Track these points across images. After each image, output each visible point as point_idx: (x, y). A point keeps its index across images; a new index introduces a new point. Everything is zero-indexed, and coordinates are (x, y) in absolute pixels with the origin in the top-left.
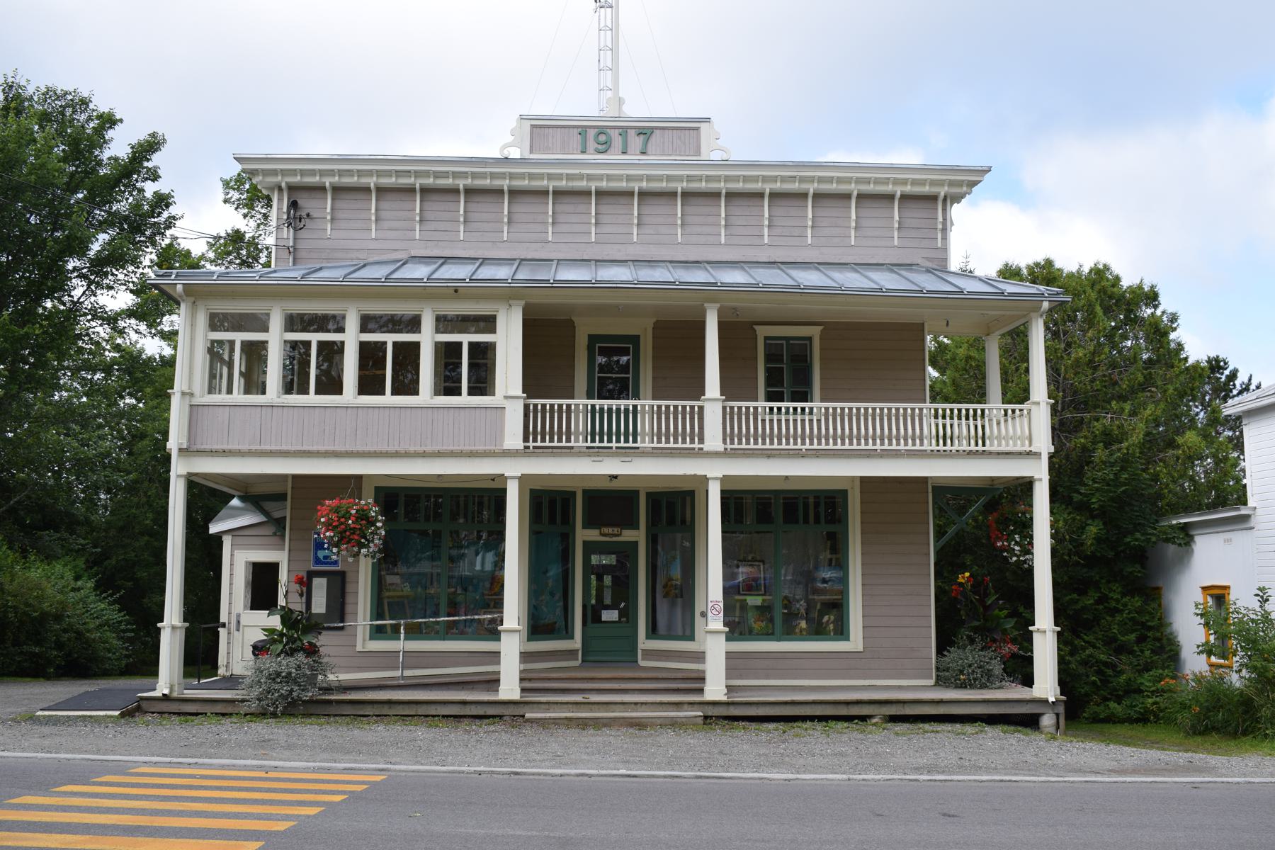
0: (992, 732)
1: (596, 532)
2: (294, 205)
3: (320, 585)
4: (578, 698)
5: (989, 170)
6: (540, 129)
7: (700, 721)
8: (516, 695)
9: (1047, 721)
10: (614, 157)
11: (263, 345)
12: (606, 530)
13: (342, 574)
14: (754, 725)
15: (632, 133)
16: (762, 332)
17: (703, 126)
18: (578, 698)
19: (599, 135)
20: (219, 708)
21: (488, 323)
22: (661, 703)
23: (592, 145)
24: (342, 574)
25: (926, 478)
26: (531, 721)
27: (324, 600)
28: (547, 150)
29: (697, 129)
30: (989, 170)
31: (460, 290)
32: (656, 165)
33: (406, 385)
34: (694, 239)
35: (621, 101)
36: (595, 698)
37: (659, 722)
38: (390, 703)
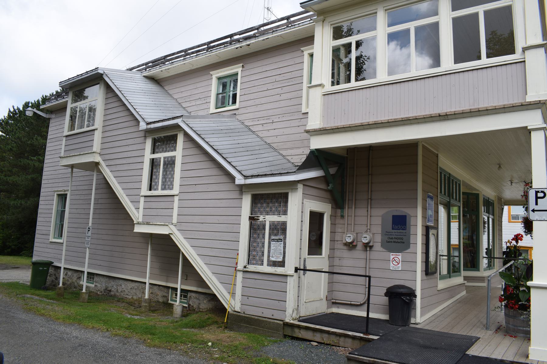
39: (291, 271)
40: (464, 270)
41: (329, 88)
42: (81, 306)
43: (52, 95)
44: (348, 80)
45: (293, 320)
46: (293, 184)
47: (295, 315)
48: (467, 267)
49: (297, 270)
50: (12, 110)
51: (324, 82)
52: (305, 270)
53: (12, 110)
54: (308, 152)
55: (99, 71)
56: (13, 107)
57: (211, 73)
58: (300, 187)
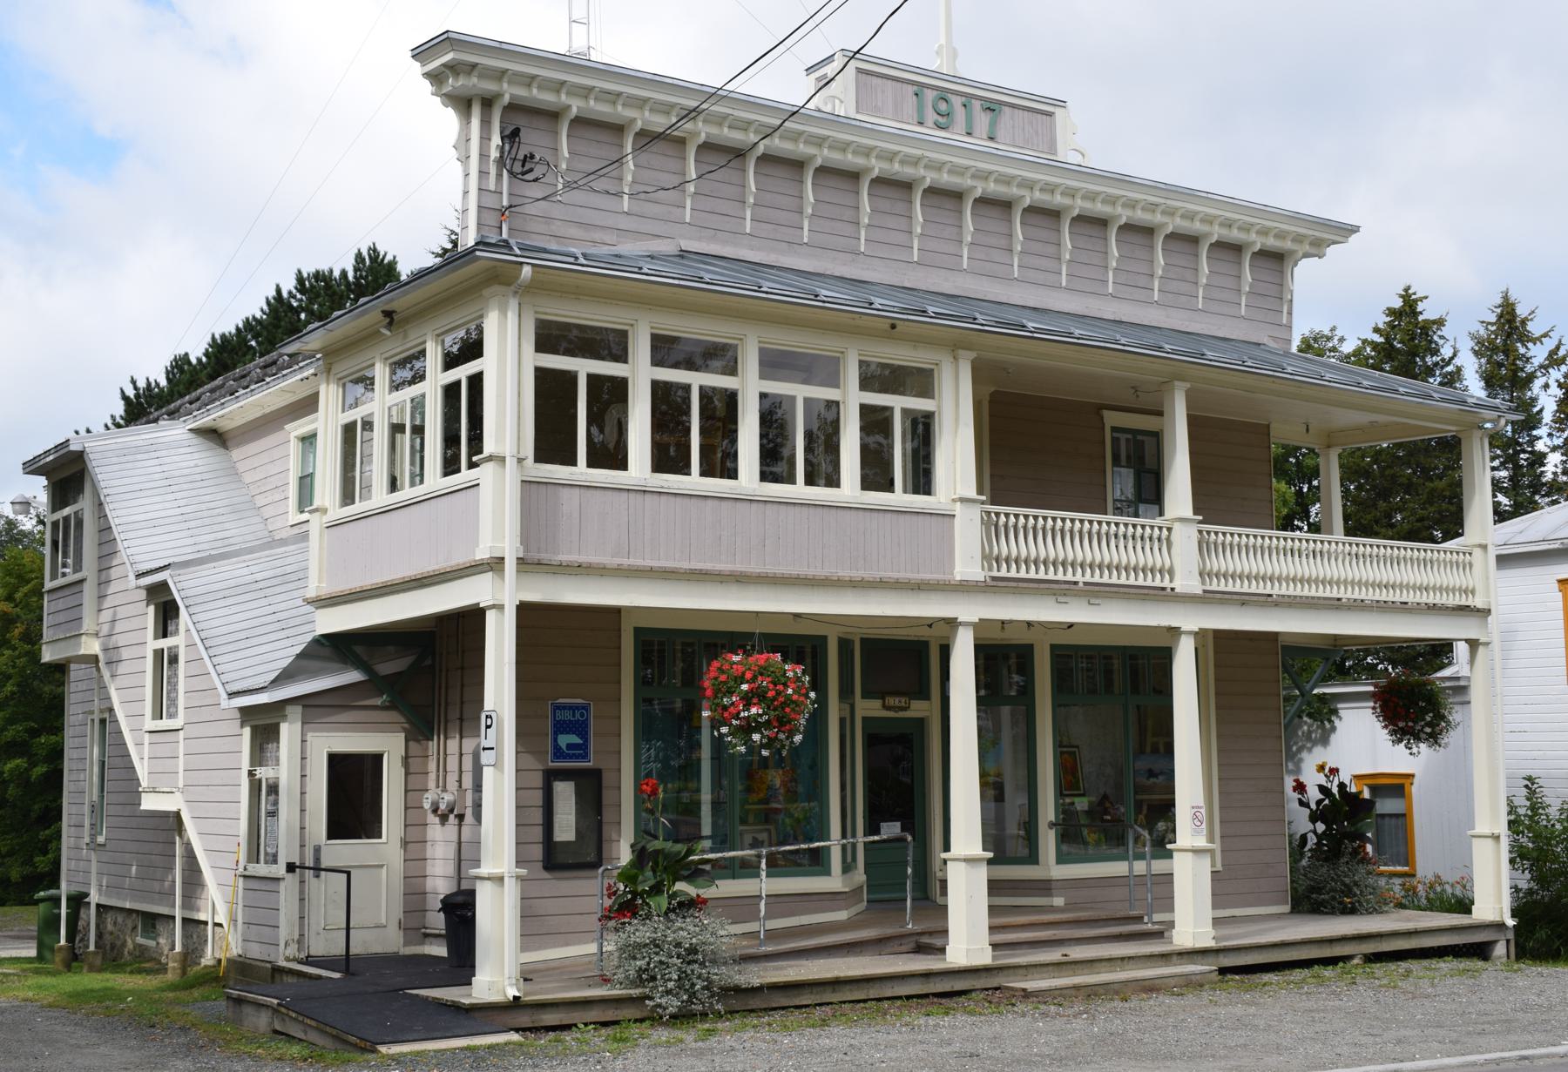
0: (1446, 965)
1: (877, 703)
2: (512, 136)
3: (565, 793)
4: (1054, 955)
5: (1354, 230)
6: (873, 74)
7: (1215, 977)
8: (985, 958)
9: (1500, 950)
10: (956, 137)
11: (731, 398)
12: (891, 701)
13: (596, 774)
14: (1246, 978)
15: (977, 104)
16: (1112, 419)
17: (1058, 111)
18: (1054, 955)
19: (941, 99)
20: (595, 1014)
21: (921, 381)
22: (1151, 957)
23: (931, 116)
24: (596, 774)
25: (1276, 634)
26: (1026, 994)
27: (572, 818)
28: (877, 111)
29: (1050, 114)
30: (1354, 230)
31: (899, 328)
32: (958, 150)
33: (823, 472)
34: (1031, 275)
35: (954, 54)
36: (1078, 953)
37: (1173, 982)
38: (836, 983)
39: (279, 870)
40: (768, 876)
41: (338, 512)
42: (668, 1044)
43: (250, 326)
44: (418, 477)
45: (288, 959)
46: (279, 707)
47: (292, 951)
48: (776, 866)
49: (291, 868)
50: (131, 393)
51: (327, 504)
52: (317, 869)
53: (131, 393)
54: (309, 638)
55: (72, 448)
56: (133, 382)
57: (287, 427)
58: (295, 712)
